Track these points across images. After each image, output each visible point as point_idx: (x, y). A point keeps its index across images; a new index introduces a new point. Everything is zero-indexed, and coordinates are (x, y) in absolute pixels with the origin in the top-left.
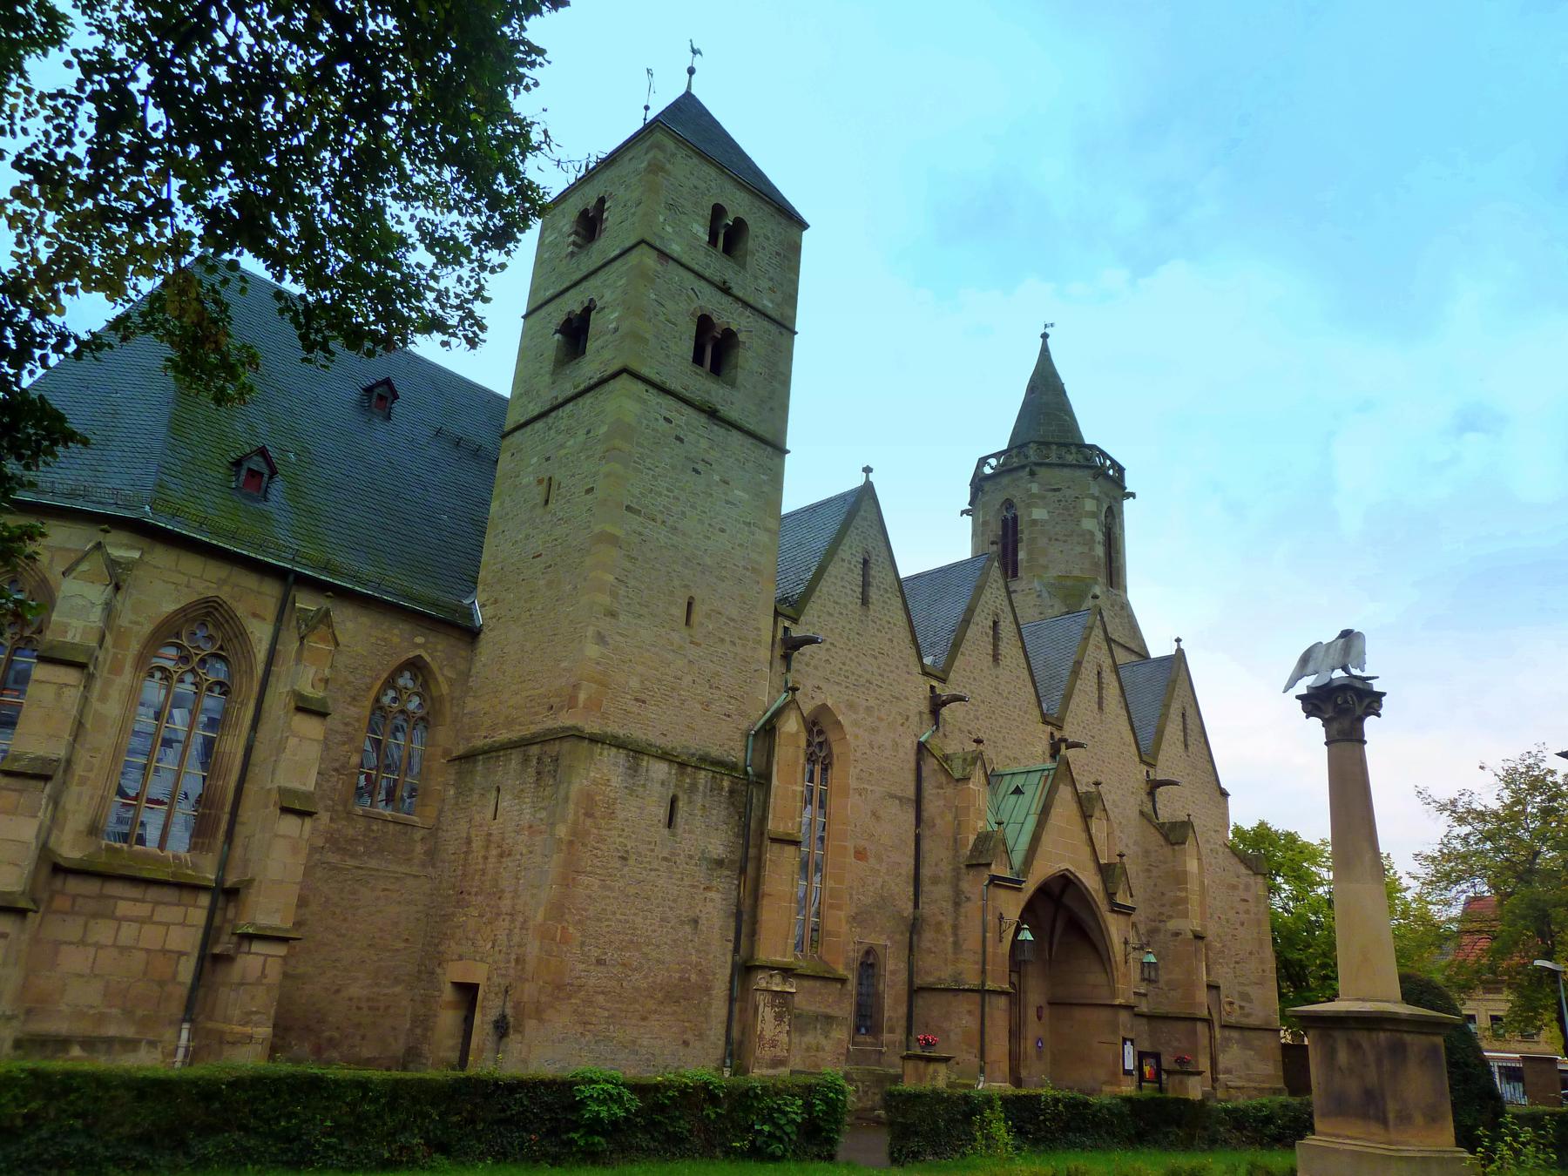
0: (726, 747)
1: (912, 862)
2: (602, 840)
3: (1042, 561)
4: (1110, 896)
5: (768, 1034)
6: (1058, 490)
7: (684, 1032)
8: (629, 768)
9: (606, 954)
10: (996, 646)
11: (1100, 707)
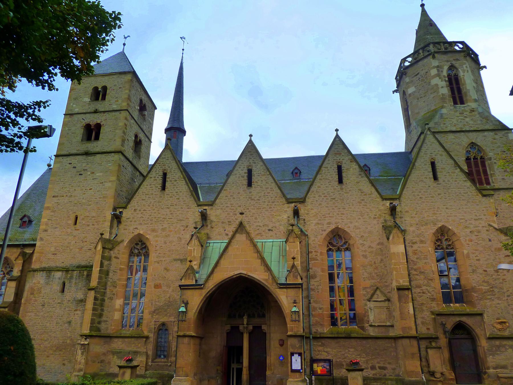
0: (88, 261)
2: (36, 301)
3: (416, 111)
5: (79, 360)
7: (64, 360)
8: (47, 277)
9: (35, 336)
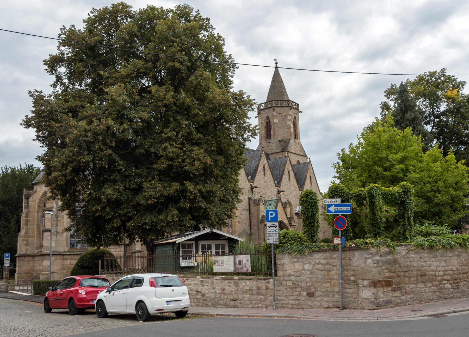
1: (249, 222)
3: (277, 134)
4: (290, 224)
6: (281, 114)
10: (264, 172)
11: (289, 180)
